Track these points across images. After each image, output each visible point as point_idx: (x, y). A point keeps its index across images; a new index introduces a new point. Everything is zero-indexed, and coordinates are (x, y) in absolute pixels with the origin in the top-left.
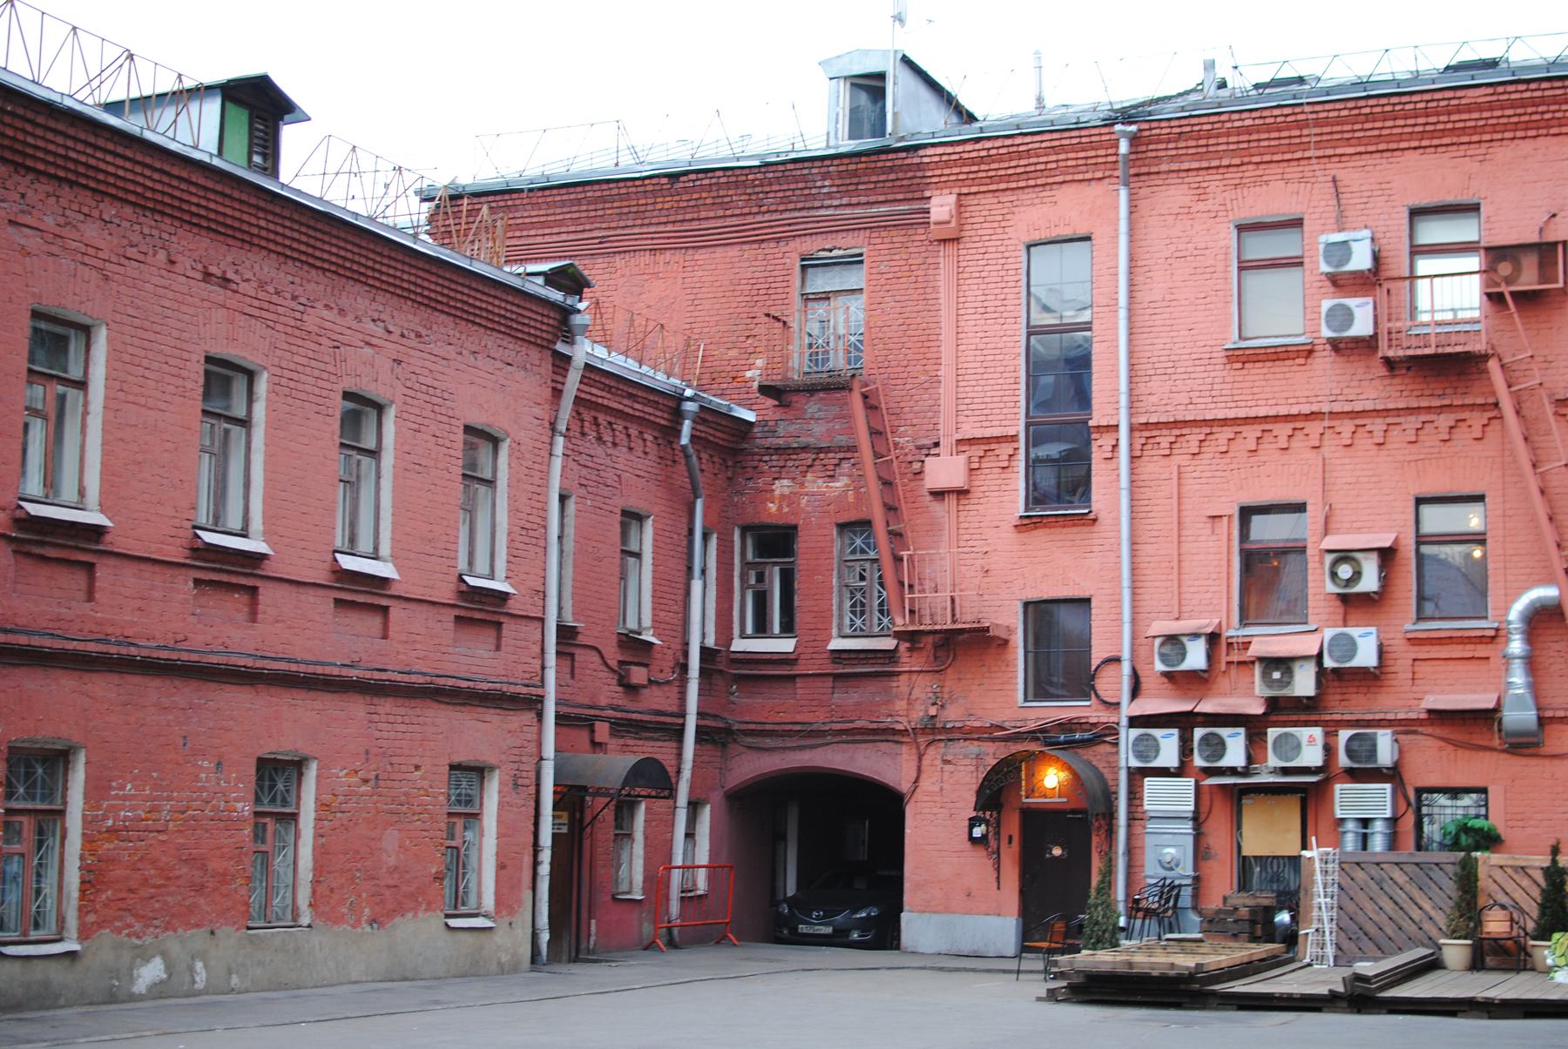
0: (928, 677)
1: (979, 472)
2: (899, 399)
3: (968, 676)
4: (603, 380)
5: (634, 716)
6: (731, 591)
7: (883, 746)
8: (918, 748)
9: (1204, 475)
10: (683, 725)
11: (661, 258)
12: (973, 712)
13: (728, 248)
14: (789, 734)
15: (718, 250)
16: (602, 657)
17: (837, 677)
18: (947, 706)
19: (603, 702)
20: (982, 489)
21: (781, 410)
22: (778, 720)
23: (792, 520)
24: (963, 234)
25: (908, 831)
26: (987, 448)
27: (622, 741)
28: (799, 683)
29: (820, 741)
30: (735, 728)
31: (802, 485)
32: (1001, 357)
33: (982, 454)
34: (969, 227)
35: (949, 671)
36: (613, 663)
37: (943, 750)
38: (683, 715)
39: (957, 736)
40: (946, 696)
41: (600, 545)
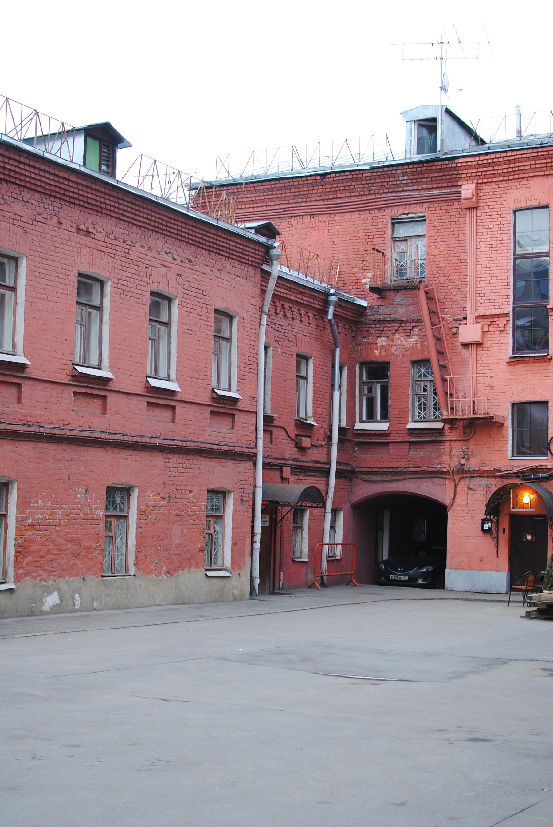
0: (460, 443)
3: (482, 443)
5: (303, 464)
8: (454, 481)
10: (329, 469)
13: (353, 214)
15: (347, 214)
17: (411, 443)
19: (287, 456)
21: (381, 300)
22: (380, 466)
23: (387, 359)
24: (479, 205)
25: (449, 526)
27: (297, 477)
31: (393, 340)
34: (482, 201)
35: (471, 440)
37: (468, 483)
40: (470, 454)
41: (285, 373)
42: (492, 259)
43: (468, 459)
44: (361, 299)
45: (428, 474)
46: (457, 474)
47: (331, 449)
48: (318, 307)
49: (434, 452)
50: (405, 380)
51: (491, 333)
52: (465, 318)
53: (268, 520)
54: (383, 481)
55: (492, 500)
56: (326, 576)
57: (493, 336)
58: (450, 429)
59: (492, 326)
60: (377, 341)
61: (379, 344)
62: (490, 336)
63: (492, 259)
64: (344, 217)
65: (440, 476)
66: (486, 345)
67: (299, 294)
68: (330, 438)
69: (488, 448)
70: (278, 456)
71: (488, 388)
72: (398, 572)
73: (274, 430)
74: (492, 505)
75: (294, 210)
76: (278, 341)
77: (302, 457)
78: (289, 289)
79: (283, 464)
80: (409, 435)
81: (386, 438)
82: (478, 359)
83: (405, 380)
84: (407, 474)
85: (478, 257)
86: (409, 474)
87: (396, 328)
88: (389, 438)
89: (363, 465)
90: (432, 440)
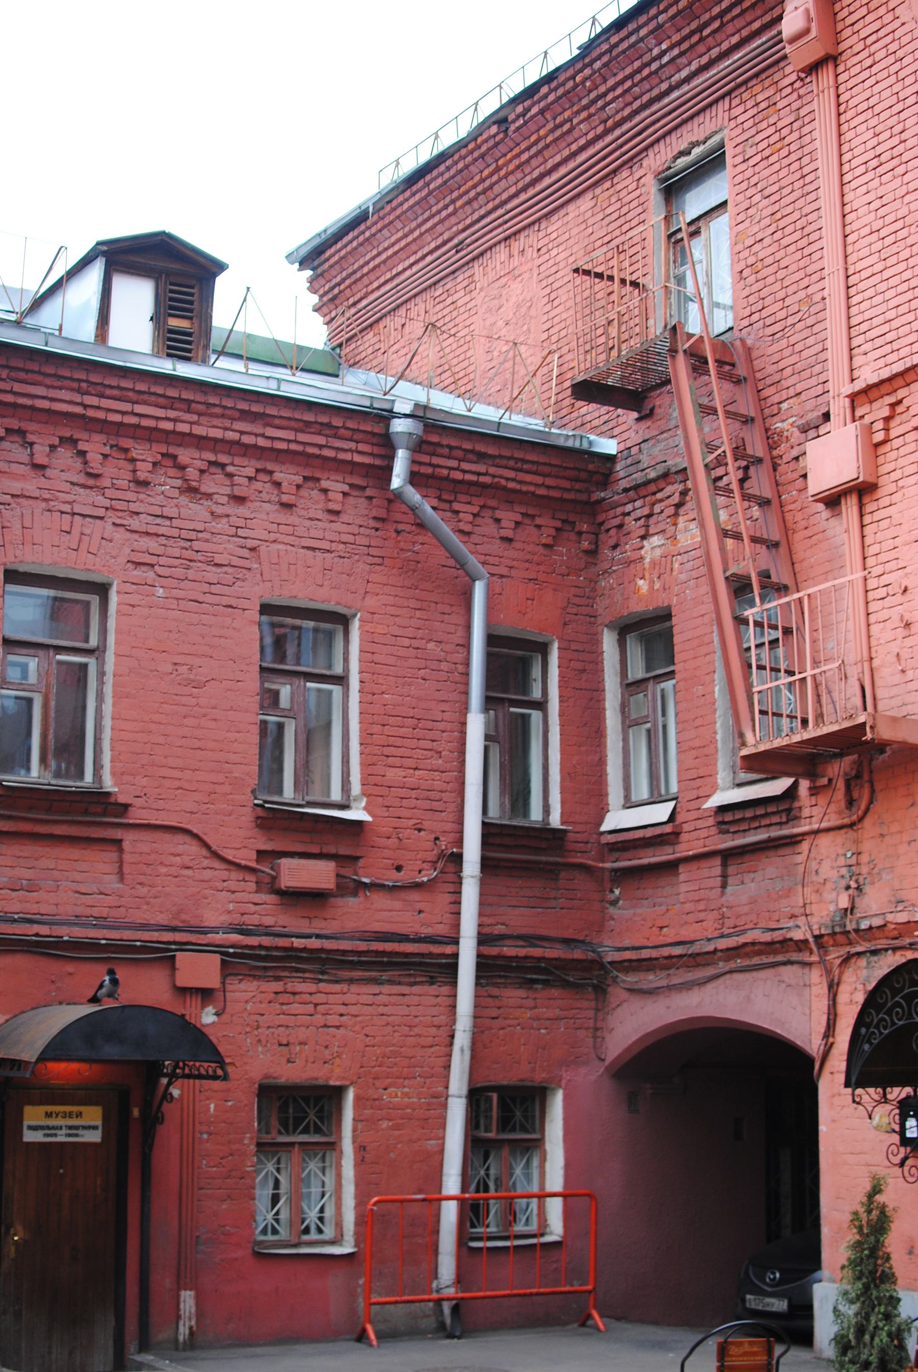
0: (840, 837)
1: (887, 447)
2: (776, 357)
3: (895, 828)
4: (297, 415)
5: (297, 943)
6: (599, 733)
7: (788, 972)
8: (828, 972)
9: (790, 188)
10: (456, 956)
11: (516, 246)
12: (903, 895)
13: (579, 202)
14: (668, 963)
15: (571, 207)
16: (207, 846)
17: (728, 856)
18: (867, 889)
19: (211, 918)
20: (894, 476)
21: (644, 425)
22: (661, 940)
23: (661, 600)
24: (842, 46)
25: (822, 1128)
26: (891, 399)
27: (277, 986)
28: (684, 873)
29: (710, 971)
30: (609, 959)
31: (674, 538)
32: (904, 233)
33: (886, 412)
34: (848, 32)
35: (867, 822)
36: (247, 857)
37: (865, 972)
38: (456, 941)
39: (881, 943)
40: (864, 870)
41: (197, 661)
42: (885, 200)
43: (858, 888)
44: (605, 437)
45: (759, 953)
46: (836, 945)
47: (460, 893)
48: (366, 460)
49: (782, 877)
50: (706, 655)
51: (896, 443)
52: (826, 417)
53: (99, 1123)
54: (670, 988)
55: (863, 1030)
56: (448, 1299)
57: (903, 451)
58: (814, 791)
59: (897, 420)
60: (643, 552)
61: (647, 560)
62: (893, 455)
63: (885, 200)
64: (566, 219)
65: (795, 956)
66: (886, 486)
67: (239, 419)
68: (457, 859)
69: (909, 843)
70: (162, 919)
71: (901, 632)
72: (767, 1285)
73: (129, 839)
74: (866, 1047)
75: (477, 240)
76: (152, 566)
77: (306, 922)
78: (185, 407)
79: (175, 943)
80: (722, 832)
81: (669, 849)
82: (868, 541)
83: (706, 655)
84: (720, 959)
85: (847, 209)
86: (727, 959)
87: (676, 499)
88: (679, 848)
89: (627, 943)
90: (770, 840)
